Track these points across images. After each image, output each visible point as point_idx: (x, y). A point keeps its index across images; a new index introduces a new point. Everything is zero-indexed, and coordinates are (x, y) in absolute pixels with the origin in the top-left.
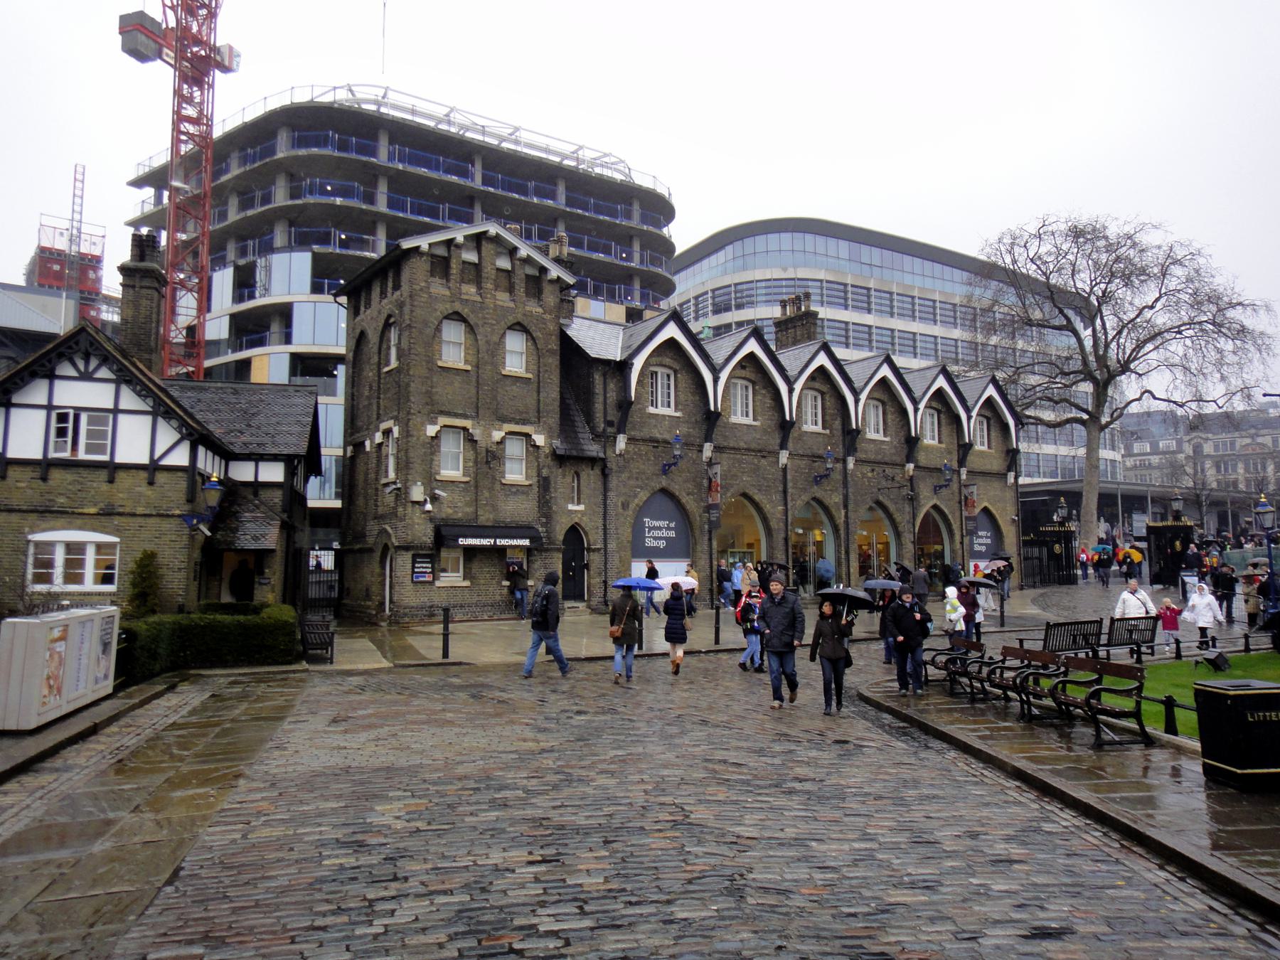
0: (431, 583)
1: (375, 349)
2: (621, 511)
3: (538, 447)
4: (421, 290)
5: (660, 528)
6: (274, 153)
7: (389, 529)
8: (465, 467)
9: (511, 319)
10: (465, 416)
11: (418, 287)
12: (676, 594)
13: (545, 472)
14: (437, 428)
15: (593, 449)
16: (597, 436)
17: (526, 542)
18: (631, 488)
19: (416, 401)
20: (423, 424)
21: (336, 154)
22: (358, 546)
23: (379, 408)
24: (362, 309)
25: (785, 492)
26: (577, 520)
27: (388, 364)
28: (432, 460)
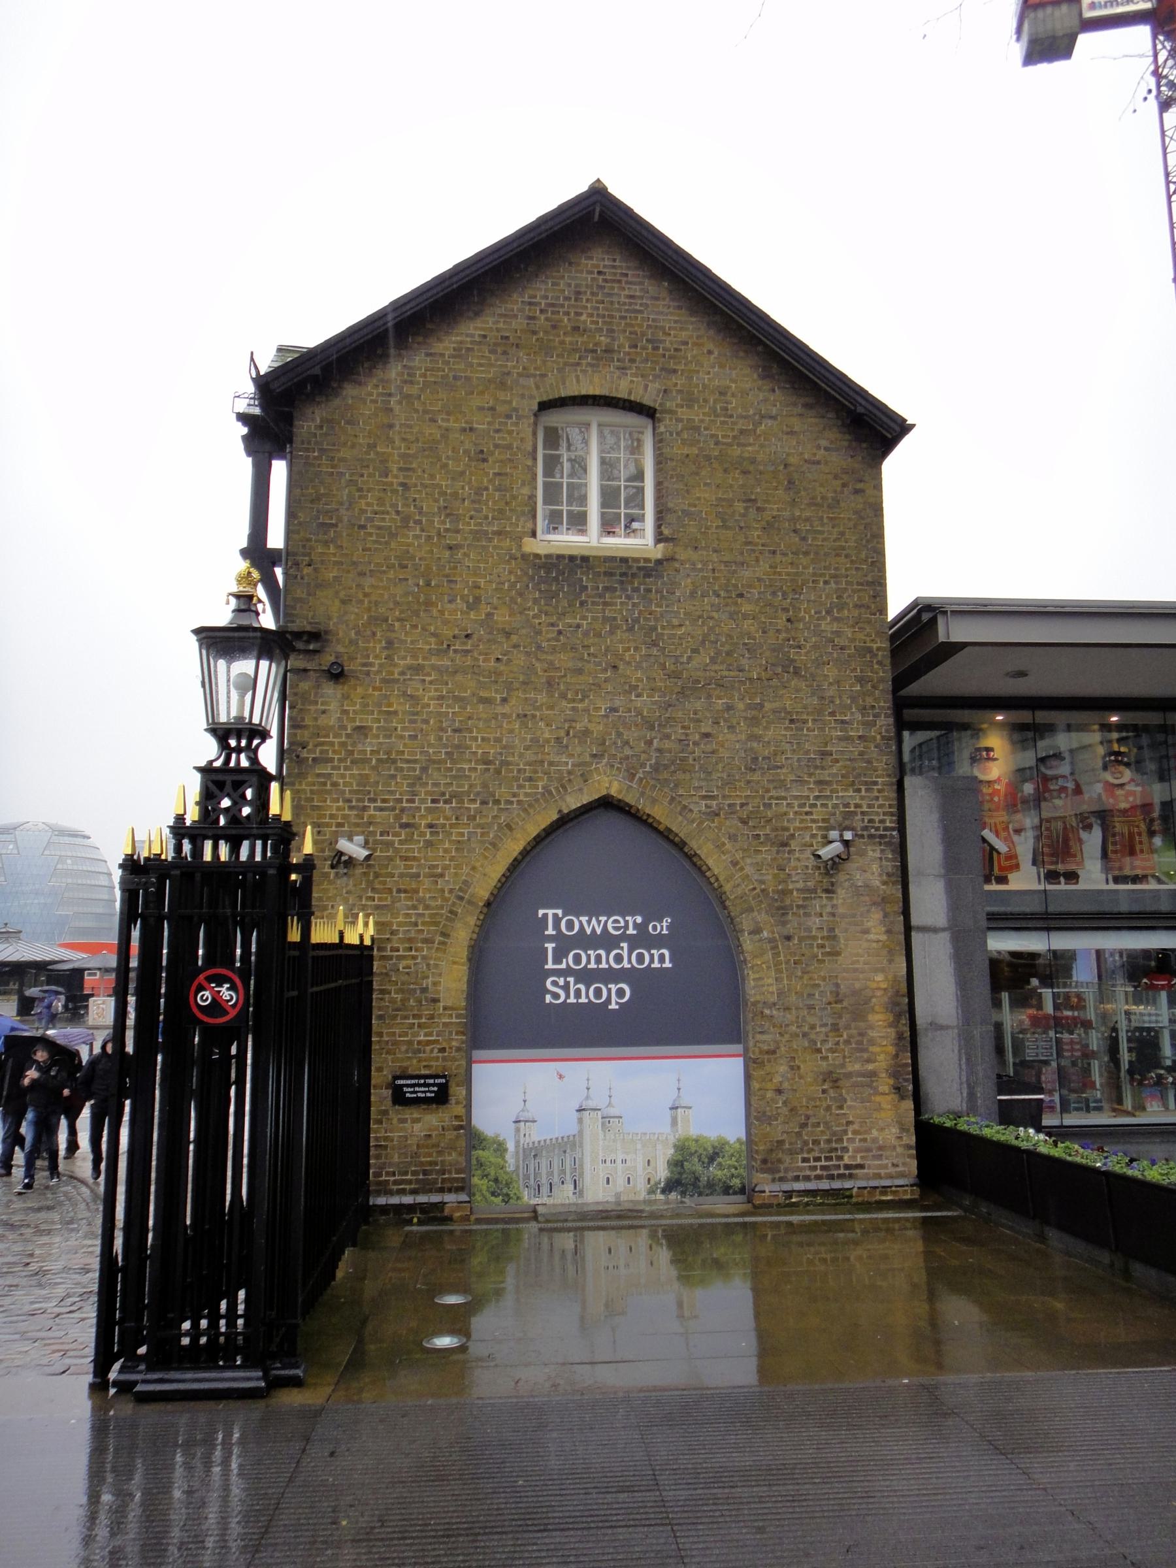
5: (607, 941)
12: (220, 733)
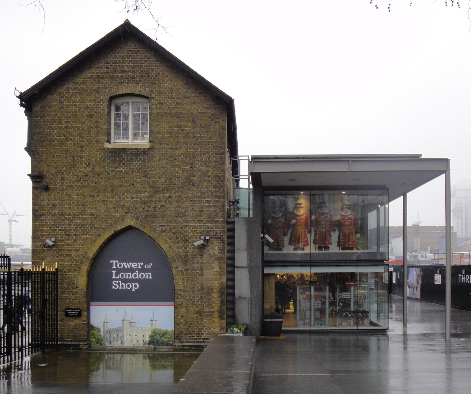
5: (132, 270)
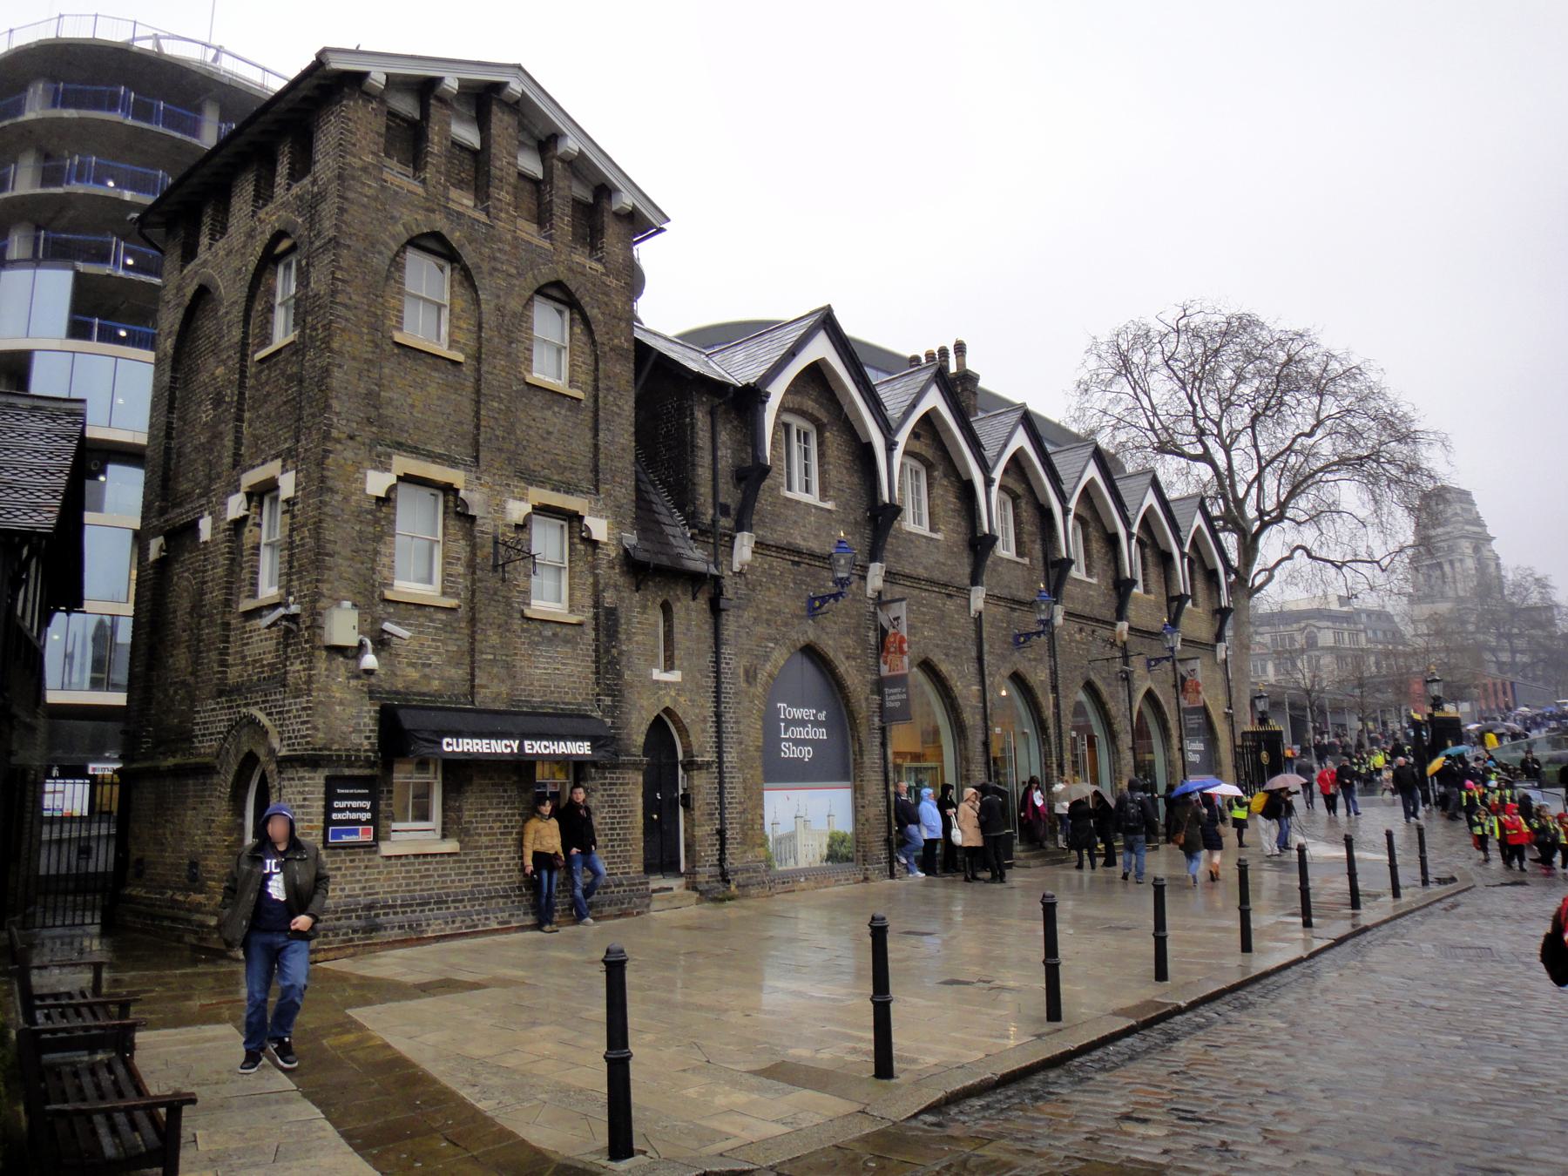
0: (371, 847)
1: (237, 313)
2: (744, 685)
3: (594, 544)
4: (364, 169)
5: (802, 723)
6: (19, 110)
7: (261, 717)
8: (447, 576)
9: (546, 274)
10: (452, 463)
11: (357, 163)
13: (609, 598)
14: (390, 479)
15: (696, 558)
16: (704, 533)
17: (582, 748)
18: (762, 638)
19: (344, 412)
20: (358, 466)
21: (129, 121)
22: (171, 762)
23: (238, 441)
24: (204, 240)
25: (980, 659)
26: (668, 702)
27: (266, 339)
28: (376, 552)
